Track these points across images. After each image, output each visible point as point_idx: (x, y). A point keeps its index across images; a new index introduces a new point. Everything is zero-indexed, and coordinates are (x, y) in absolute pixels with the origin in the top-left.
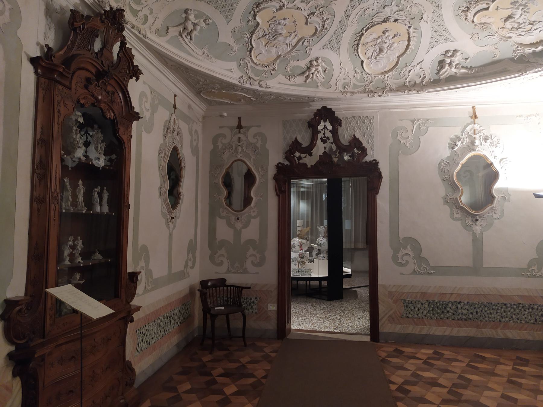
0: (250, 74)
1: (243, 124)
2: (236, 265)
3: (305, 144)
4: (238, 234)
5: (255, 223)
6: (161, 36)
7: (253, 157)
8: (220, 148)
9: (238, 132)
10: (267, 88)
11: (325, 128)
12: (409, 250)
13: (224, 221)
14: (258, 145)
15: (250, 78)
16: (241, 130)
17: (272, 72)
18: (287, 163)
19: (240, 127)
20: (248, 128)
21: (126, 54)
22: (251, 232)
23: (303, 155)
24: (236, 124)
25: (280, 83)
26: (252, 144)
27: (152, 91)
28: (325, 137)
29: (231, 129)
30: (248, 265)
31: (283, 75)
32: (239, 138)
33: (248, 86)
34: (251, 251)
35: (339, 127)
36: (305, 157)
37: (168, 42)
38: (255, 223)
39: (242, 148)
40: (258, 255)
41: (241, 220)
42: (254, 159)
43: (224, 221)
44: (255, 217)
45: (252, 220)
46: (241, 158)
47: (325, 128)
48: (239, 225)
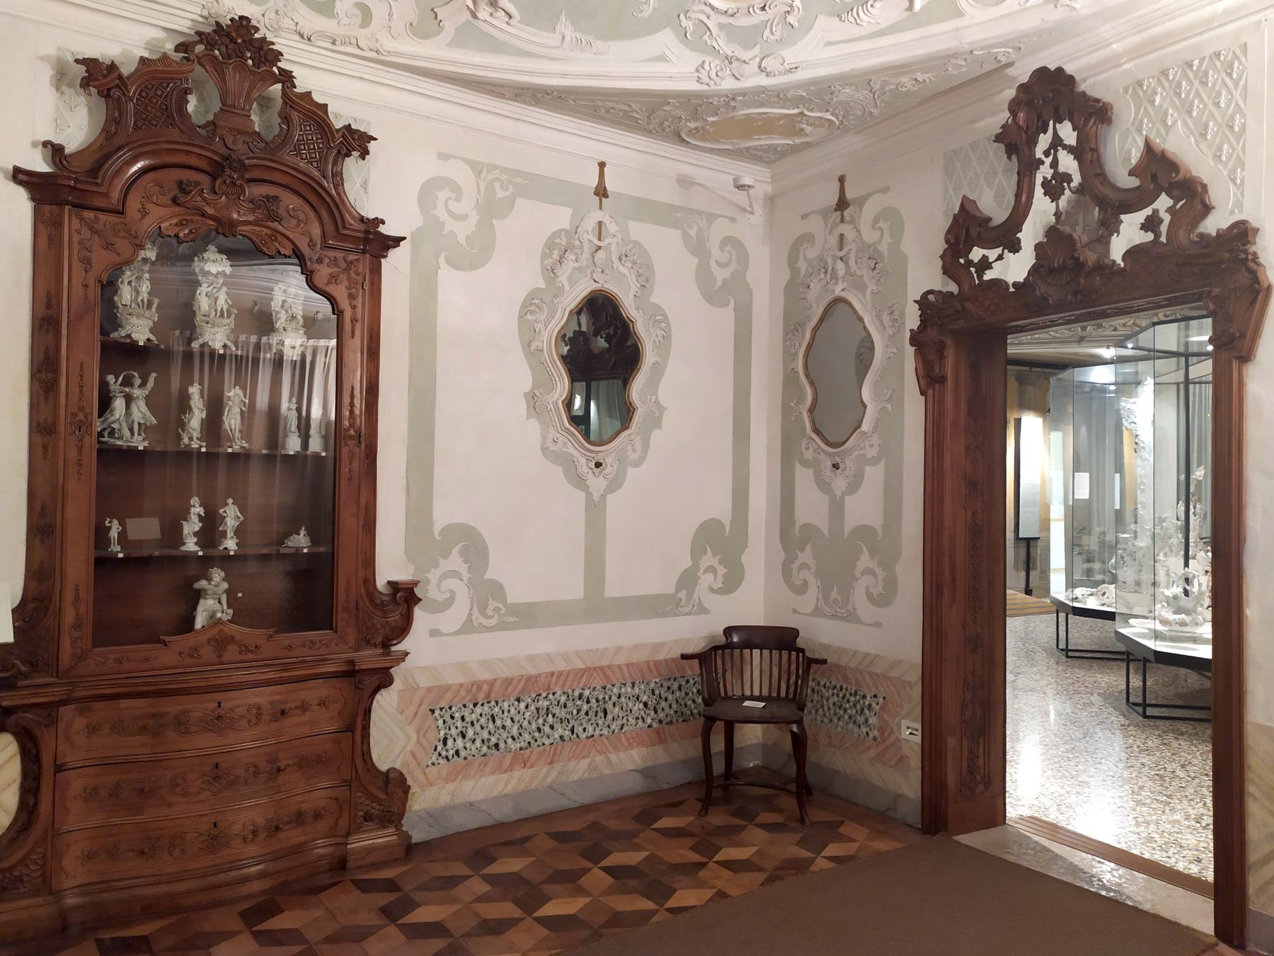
0: (726, 48)
1: (850, 195)
2: (834, 594)
3: (999, 215)
4: (837, 509)
5: (875, 475)
6: (426, 37)
7: (871, 286)
8: (803, 272)
9: (838, 220)
10: (790, 71)
11: (1057, 142)
12: (455, 561)
13: (810, 472)
14: (884, 248)
15: (729, 60)
16: (846, 213)
17: (790, 19)
18: (953, 288)
19: (842, 204)
20: (861, 202)
21: (308, 113)
22: (864, 508)
23: (992, 254)
24: (834, 199)
25: (829, 44)
26: (869, 246)
27: (477, 168)
28: (1056, 175)
29: (824, 213)
30: (859, 598)
31: (831, 14)
32: (842, 236)
33: (728, 84)
34: (865, 561)
35: (1102, 128)
36: (1000, 258)
37: (454, 44)
38: (875, 475)
39: (847, 264)
40: (881, 573)
41: (844, 470)
42: (873, 293)
43: (810, 472)
44: (874, 461)
45: (868, 469)
46: (844, 294)
47: (1057, 142)
48: (839, 483)
